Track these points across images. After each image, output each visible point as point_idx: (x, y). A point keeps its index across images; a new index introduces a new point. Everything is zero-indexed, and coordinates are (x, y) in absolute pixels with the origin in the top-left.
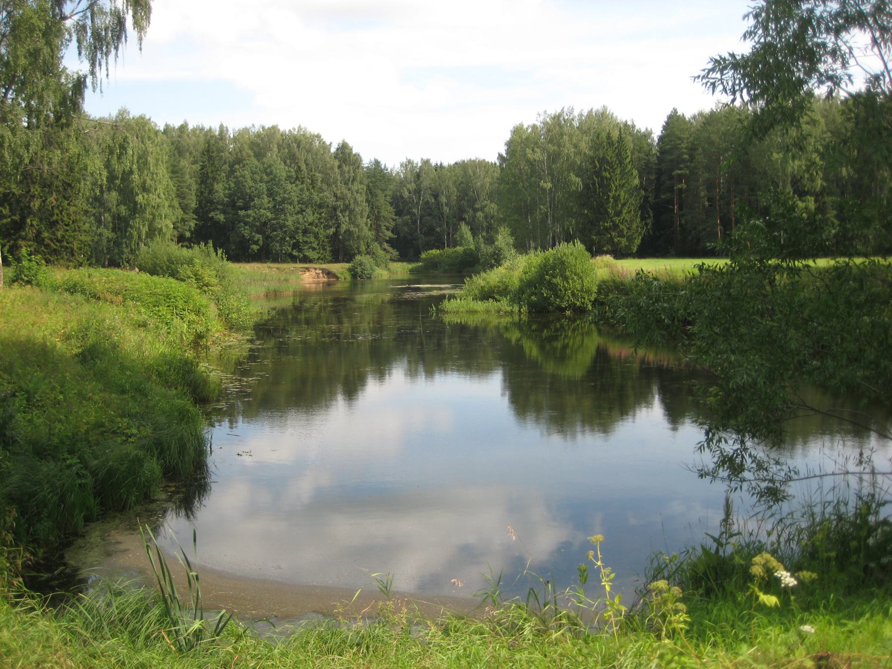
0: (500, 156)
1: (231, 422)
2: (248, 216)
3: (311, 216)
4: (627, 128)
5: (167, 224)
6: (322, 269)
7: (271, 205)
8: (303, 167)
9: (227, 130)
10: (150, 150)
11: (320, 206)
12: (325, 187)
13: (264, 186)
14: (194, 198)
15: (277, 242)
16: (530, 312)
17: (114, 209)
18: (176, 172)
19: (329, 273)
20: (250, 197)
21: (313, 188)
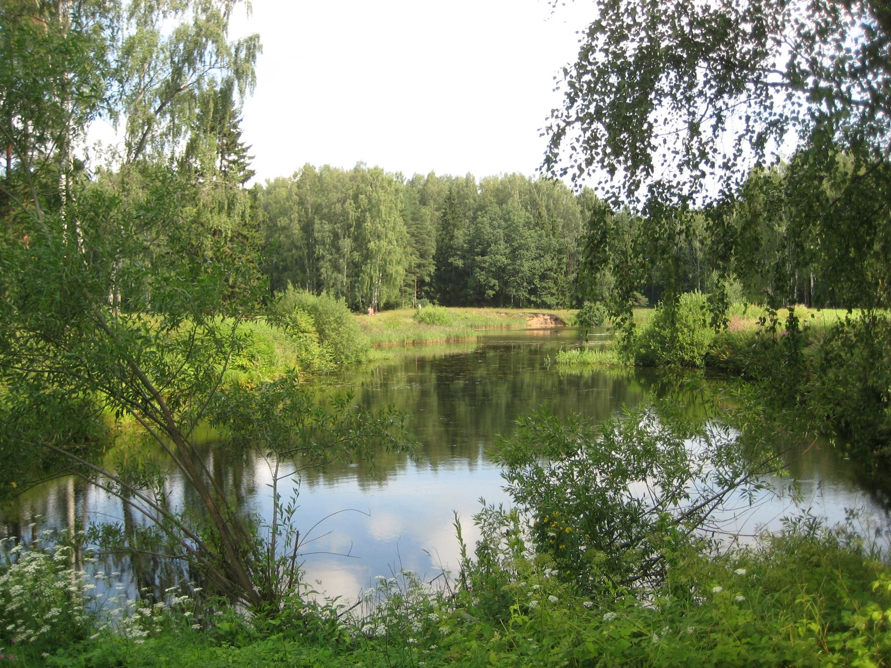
1: (470, 464)
2: (485, 262)
3: (549, 262)
5: (398, 271)
6: (550, 315)
7: (507, 251)
8: (544, 213)
9: (474, 178)
10: (382, 198)
11: (560, 252)
12: (566, 232)
13: (501, 231)
14: (434, 244)
15: (514, 287)
16: (637, 365)
17: (348, 255)
18: (417, 220)
19: (556, 319)
20: (488, 243)
21: (554, 234)
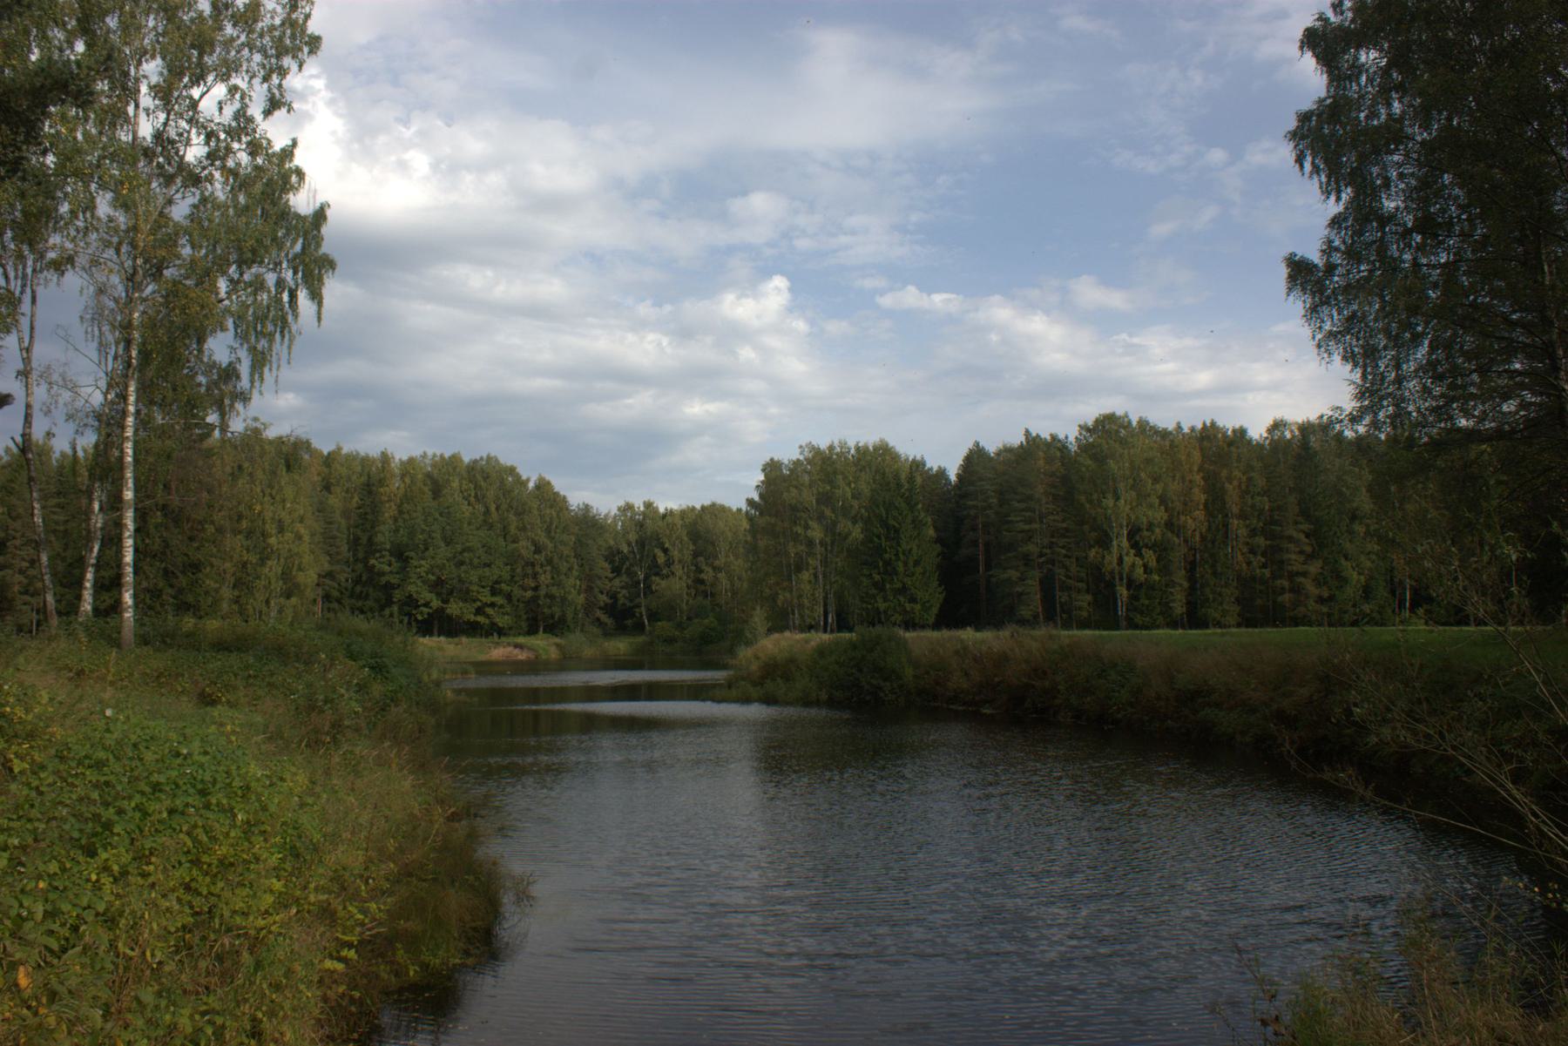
0: (750, 502)
4: (917, 465)
8: (493, 508)
